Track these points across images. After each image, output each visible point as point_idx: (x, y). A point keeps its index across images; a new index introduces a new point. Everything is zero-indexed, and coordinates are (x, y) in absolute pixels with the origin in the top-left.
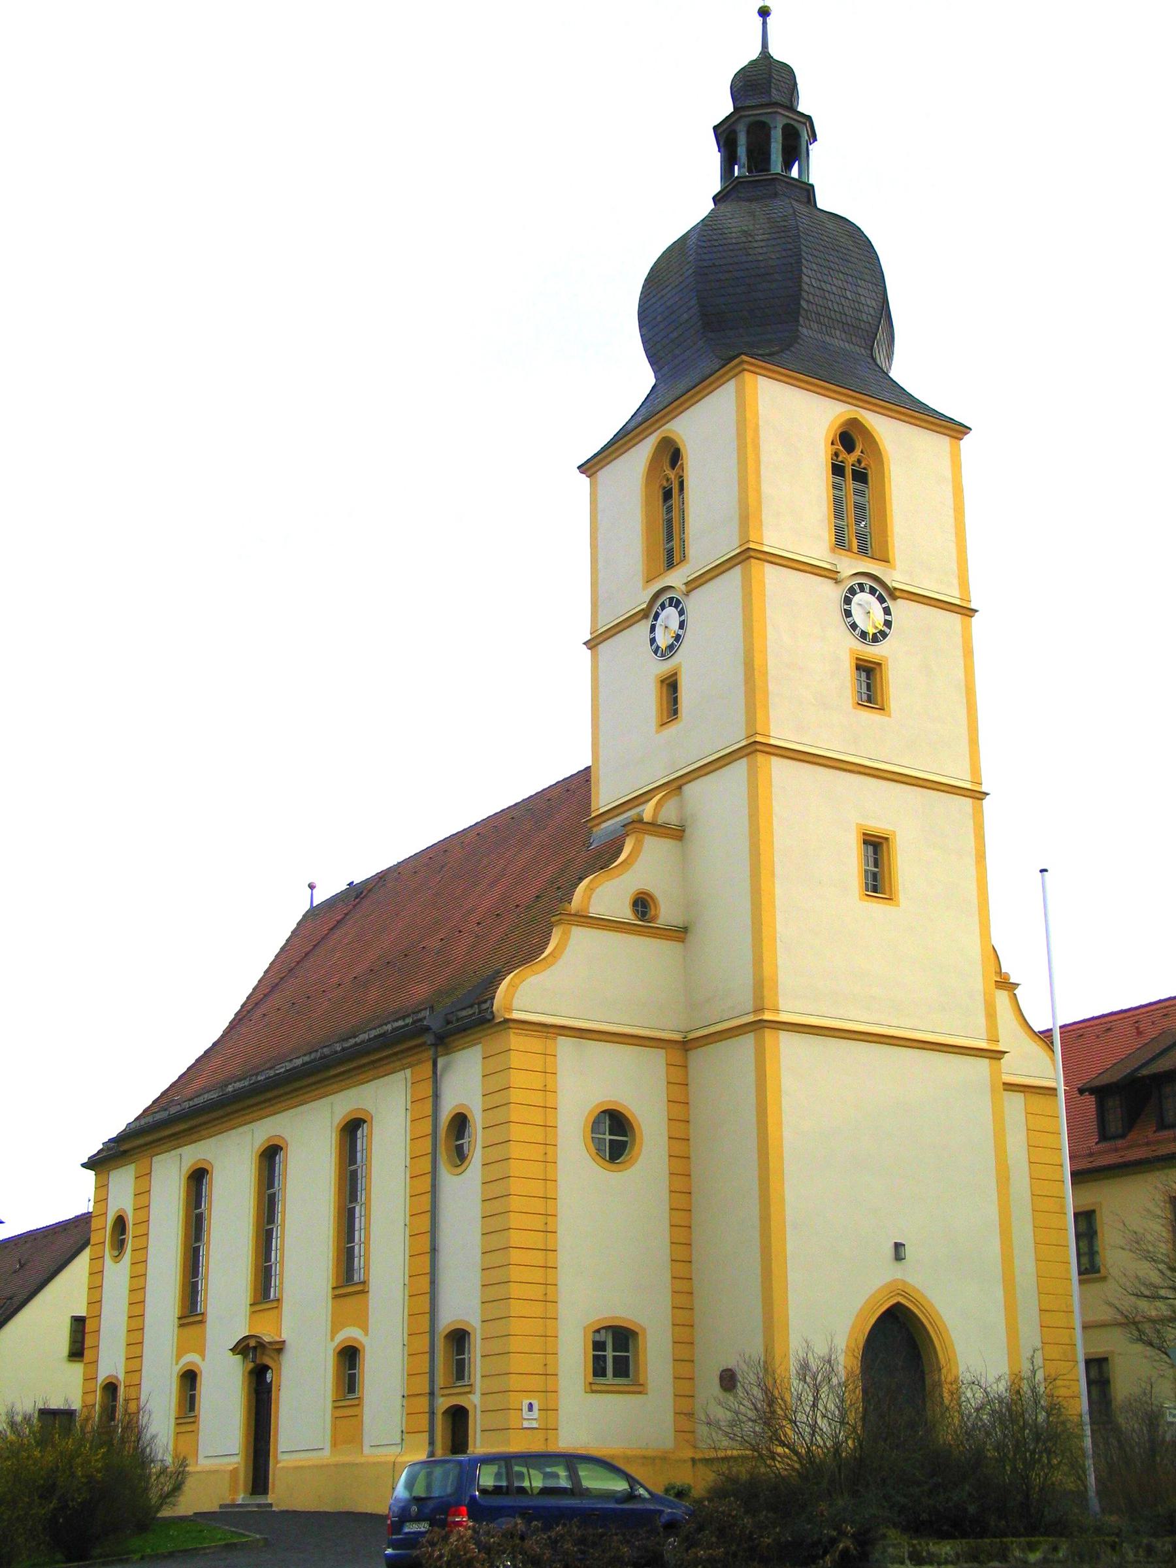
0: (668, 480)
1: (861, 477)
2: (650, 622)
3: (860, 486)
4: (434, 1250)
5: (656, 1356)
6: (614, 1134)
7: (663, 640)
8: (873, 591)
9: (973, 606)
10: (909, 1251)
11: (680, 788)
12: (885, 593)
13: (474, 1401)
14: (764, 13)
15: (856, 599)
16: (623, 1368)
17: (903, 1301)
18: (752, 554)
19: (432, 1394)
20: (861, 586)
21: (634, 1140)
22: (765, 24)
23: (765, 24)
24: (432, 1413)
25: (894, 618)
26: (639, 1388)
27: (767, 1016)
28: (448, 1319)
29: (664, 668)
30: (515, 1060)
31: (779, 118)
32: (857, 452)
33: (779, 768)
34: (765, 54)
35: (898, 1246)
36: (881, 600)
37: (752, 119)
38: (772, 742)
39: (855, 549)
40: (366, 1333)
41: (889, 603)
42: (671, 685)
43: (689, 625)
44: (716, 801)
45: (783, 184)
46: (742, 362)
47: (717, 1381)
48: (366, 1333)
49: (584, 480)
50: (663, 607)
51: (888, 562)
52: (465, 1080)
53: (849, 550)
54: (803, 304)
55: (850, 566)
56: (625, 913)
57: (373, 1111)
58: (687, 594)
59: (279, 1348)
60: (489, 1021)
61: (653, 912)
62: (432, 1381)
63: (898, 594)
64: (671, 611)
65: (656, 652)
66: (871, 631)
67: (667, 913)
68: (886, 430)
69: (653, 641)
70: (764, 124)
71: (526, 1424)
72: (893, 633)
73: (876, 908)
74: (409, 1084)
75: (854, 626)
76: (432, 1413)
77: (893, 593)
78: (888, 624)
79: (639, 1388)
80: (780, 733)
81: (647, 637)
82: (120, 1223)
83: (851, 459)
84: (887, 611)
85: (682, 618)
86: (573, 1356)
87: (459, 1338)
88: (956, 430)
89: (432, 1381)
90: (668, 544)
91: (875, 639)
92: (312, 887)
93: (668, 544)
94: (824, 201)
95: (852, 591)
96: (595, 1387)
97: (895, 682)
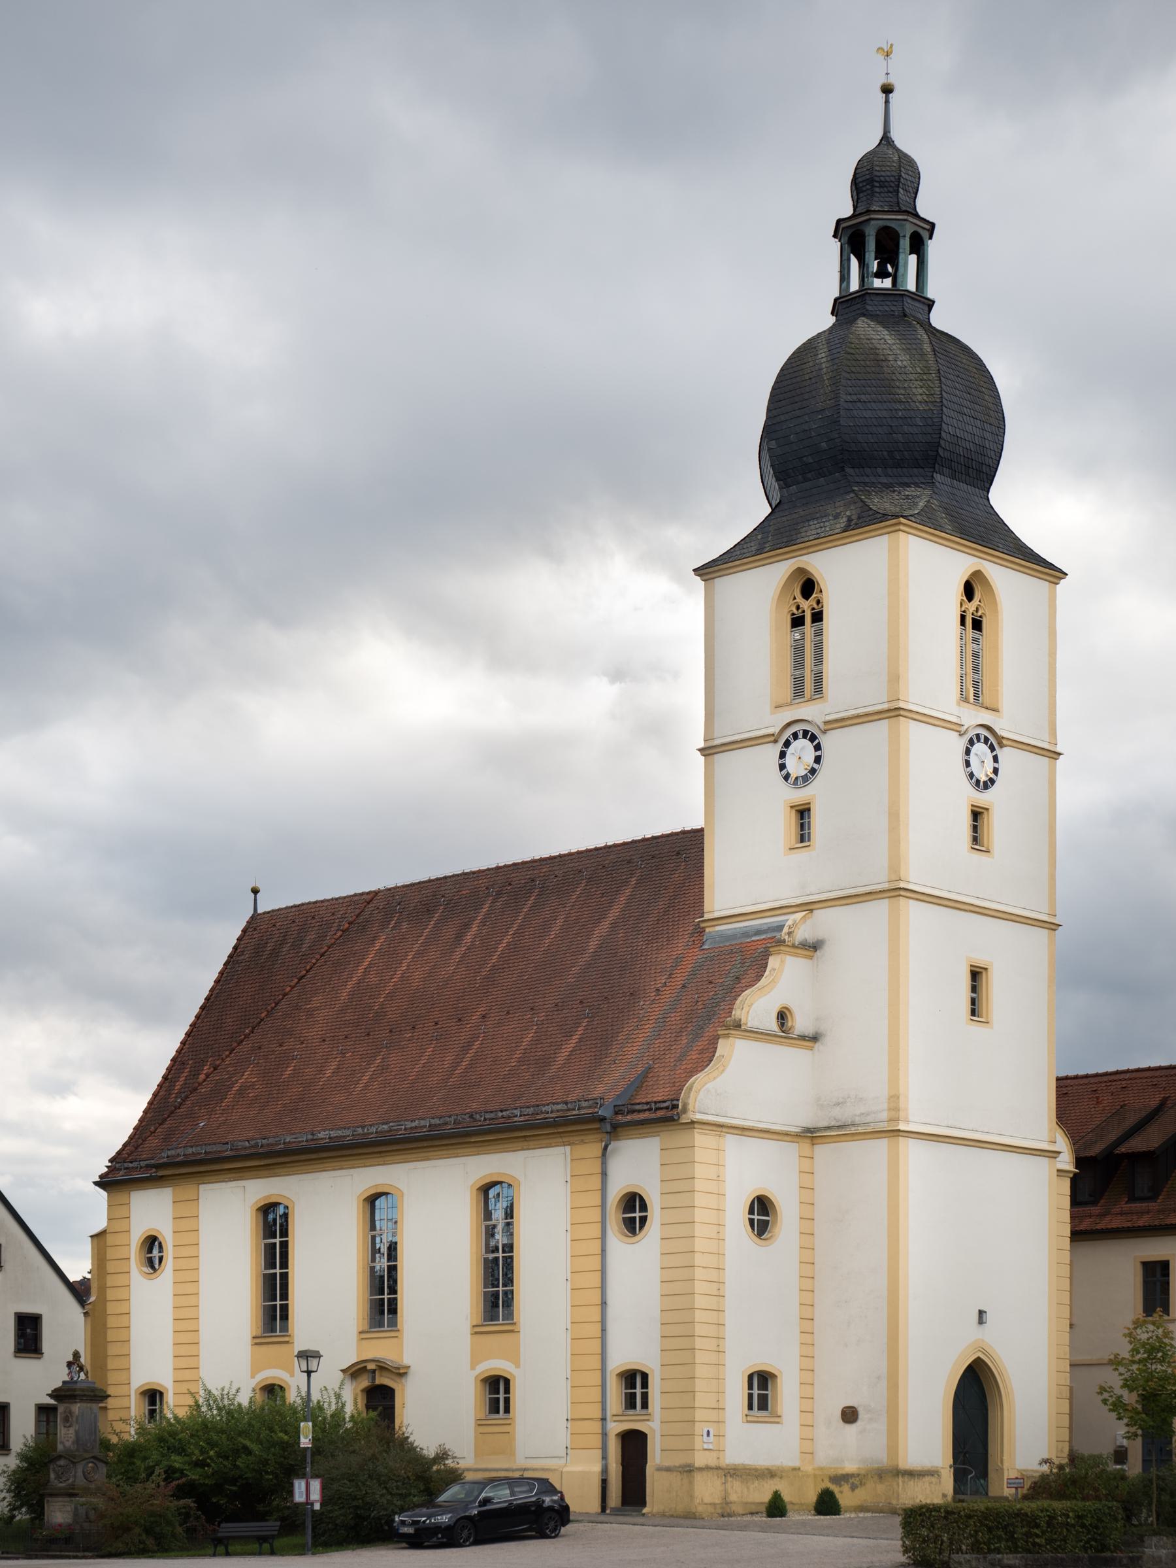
0: (798, 608)
1: (977, 625)
2: (779, 746)
3: (977, 634)
4: (604, 1303)
5: (787, 1393)
6: (762, 1212)
7: (795, 768)
8: (986, 740)
9: (1059, 750)
10: (989, 1317)
11: (811, 910)
12: (993, 740)
13: (653, 1425)
14: (887, 90)
15: (974, 750)
16: (764, 1404)
17: (983, 1357)
18: (902, 713)
19: (604, 1419)
20: (986, 740)
21: (775, 1221)
22: (887, 102)
23: (887, 102)
24: (604, 1434)
25: (1001, 766)
26: (776, 1418)
27: (902, 1127)
28: (621, 1358)
29: (800, 796)
30: (699, 1155)
31: (908, 225)
32: (975, 602)
33: (914, 911)
34: (886, 139)
35: (981, 1313)
36: (992, 748)
37: (881, 223)
38: (911, 887)
39: (972, 700)
40: (518, 1365)
41: (998, 751)
42: (803, 813)
43: (824, 760)
44: (852, 933)
45: (909, 301)
46: (900, 523)
47: (860, 1416)
48: (518, 1365)
49: (699, 583)
50: (795, 736)
51: (997, 711)
52: (637, 1163)
53: (966, 700)
54: (941, 451)
55: (972, 717)
56: (773, 1026)
57: (521, 1179)
58: (824, 732)
59: (401, 1373)
60: (674, 1120)
61: (790, 1024)
62: (604, 1409)
63: (1005, 742)
64: (802, 744)
65: (786, 777)
66: (983, 778)
67: (801, 1023)
68: (1004, 579)
69: (782, 767)
70: (883, 217)
71: (706, 1446)
72: (999, 780)
73: (976, 1029)
74: (569, 1160)
75: (971, 775)
76: (604, 1434)
77: (1001, 741)
78: (996, 771)
79: (776, 1418)
80: (915, 879)
81: (775, 761)
82: (151, 1242)
83: (971, 607)
84: (996, 759)
85: (818, 753)
86: (736, 1393)
87: (634, 1379)
88: (1052, 572)
89: (604, 1409)
90: (805, 676)
91: (986, 787)
92: (255, 891)
93: (805, 676)
94: (939, 319)
95: (971, 742)
96: (749, 1418)
97: (997, 827)
